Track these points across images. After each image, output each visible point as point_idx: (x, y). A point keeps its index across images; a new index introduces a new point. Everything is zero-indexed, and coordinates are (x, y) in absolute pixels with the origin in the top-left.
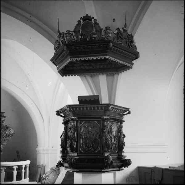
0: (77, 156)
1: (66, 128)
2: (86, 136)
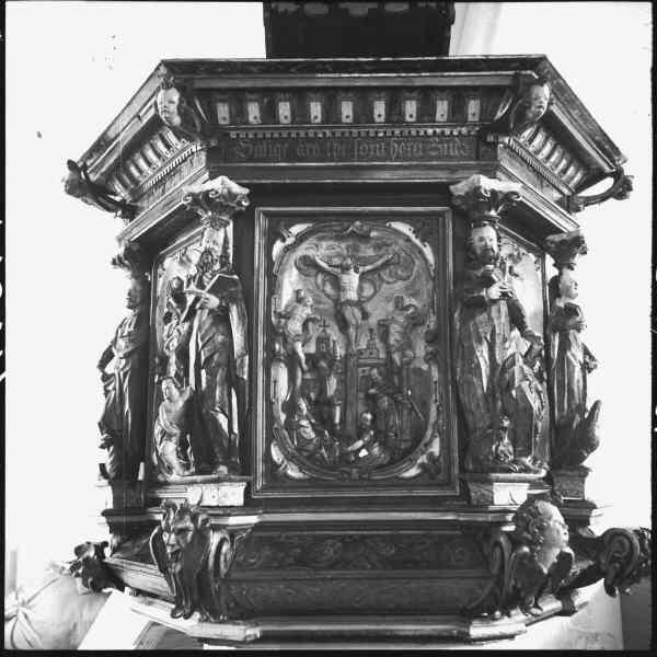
1: (142, 300)
2: (320, 341)
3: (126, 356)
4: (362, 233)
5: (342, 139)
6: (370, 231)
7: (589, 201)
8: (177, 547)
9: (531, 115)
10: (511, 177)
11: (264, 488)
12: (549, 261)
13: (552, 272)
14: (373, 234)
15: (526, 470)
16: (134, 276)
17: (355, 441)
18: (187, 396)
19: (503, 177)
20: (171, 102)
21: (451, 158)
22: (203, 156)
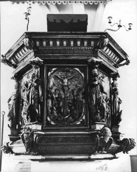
0: (43, 130)
1: (18, 87)
2: (58, 94)
3: (14, 100)
4: (68, 70)
5: (64, 50)
6: (70, 70)
7: (120, 65)
8: (27, 137)
9: (104, 45)
10: (101, 58)
11: (46, 127)
12: (112, 79)
13: (112, 81)
14: (70, 70)
15: (103, 122)
16: (16, 82)
17: (66, 116)
18: (29, 105)
19: (99, 58)
20: (27, 41)
21: (87, 54)
22: (33, 53)
